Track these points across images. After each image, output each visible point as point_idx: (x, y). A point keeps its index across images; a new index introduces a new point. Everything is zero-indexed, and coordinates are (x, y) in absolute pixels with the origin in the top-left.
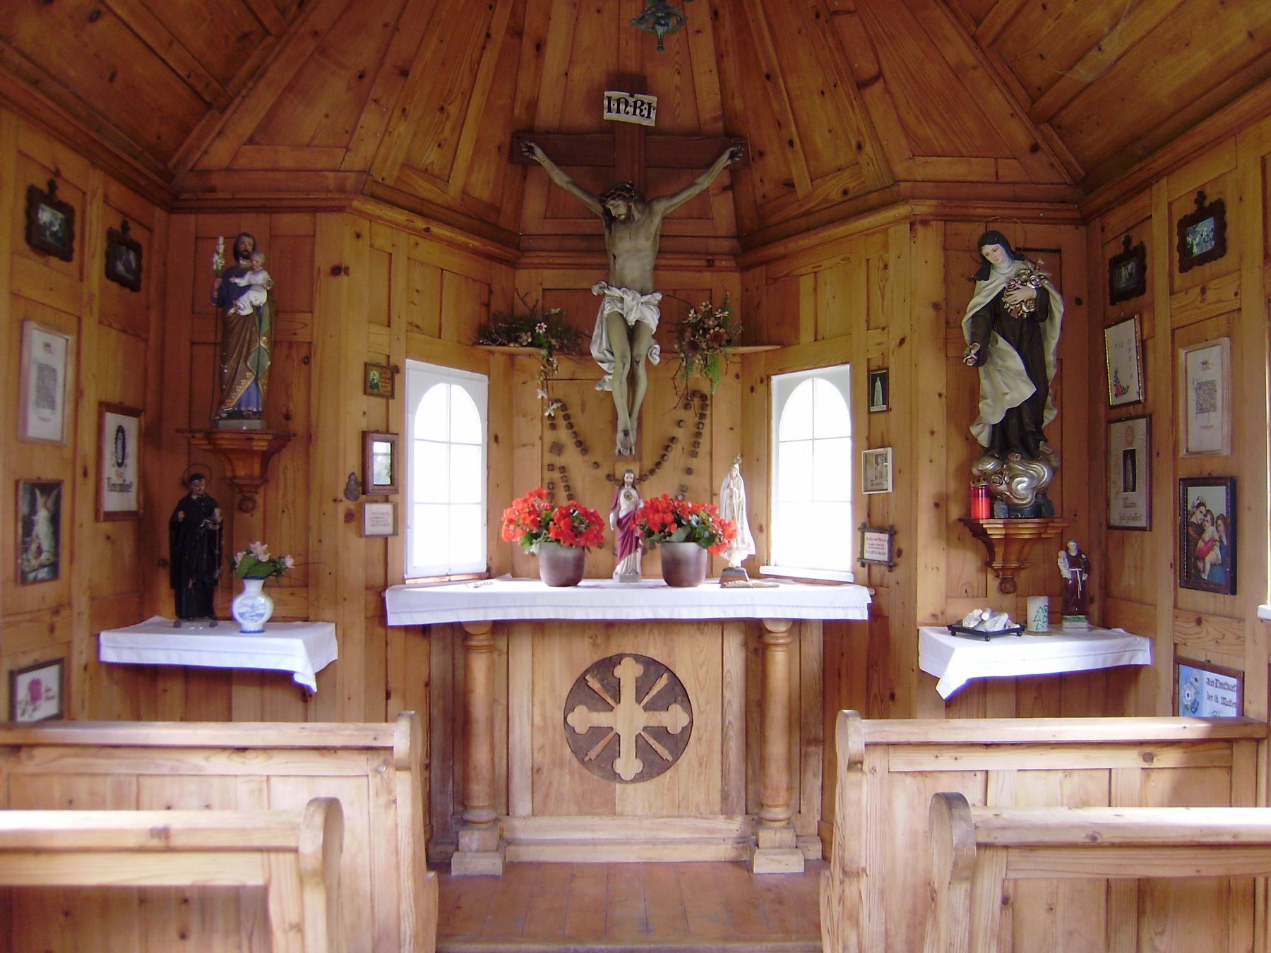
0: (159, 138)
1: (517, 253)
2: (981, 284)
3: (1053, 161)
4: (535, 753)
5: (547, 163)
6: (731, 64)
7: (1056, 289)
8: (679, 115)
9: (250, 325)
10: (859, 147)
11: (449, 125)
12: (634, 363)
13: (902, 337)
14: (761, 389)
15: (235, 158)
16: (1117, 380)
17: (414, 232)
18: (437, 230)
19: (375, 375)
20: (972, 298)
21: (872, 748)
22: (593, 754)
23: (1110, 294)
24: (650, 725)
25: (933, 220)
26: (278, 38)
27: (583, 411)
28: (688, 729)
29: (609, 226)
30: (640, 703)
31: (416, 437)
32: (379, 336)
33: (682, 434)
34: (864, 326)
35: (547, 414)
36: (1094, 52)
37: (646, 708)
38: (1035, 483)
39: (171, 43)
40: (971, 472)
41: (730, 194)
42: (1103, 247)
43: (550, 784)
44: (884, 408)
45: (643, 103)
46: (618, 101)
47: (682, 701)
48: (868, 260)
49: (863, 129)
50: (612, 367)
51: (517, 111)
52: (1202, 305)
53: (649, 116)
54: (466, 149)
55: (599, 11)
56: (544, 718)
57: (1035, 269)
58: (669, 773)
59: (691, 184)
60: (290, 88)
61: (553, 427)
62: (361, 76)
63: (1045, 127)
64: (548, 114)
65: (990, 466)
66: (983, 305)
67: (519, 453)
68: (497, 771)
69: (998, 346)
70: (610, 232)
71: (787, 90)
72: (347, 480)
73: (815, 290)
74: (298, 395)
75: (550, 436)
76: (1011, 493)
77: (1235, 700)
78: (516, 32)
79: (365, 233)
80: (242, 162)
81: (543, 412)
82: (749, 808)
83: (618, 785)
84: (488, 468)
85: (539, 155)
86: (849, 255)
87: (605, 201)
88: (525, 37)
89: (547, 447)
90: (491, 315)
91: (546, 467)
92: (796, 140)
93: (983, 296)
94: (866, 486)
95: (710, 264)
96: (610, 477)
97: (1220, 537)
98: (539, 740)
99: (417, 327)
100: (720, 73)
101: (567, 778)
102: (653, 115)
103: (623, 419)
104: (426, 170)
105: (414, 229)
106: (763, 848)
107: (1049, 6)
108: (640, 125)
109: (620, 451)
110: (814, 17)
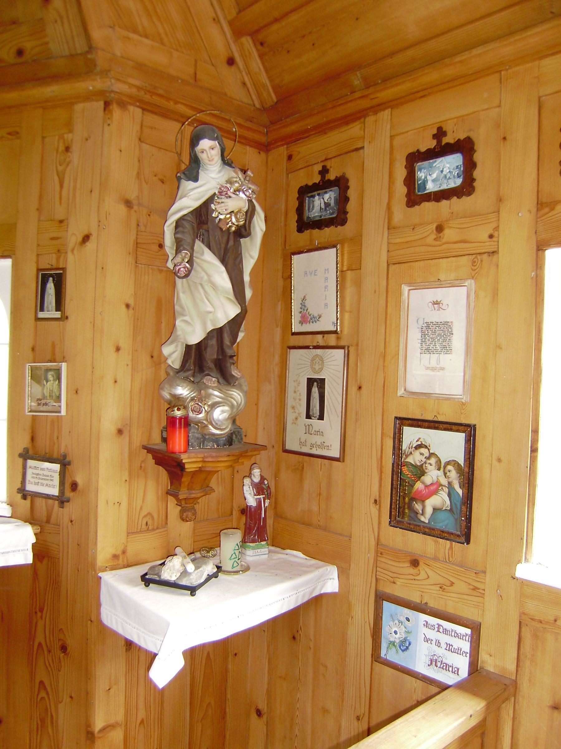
3: (247, 79)
13: (86, 232)
16: (303, 306)
25: (131, 104)
40: (161, 396)
52: (438, 243)
57: (245, 179)
63: (247, 41)
66: (191, 209)
77: (467, 649)
86: (18, 129)
97: (450, 483)
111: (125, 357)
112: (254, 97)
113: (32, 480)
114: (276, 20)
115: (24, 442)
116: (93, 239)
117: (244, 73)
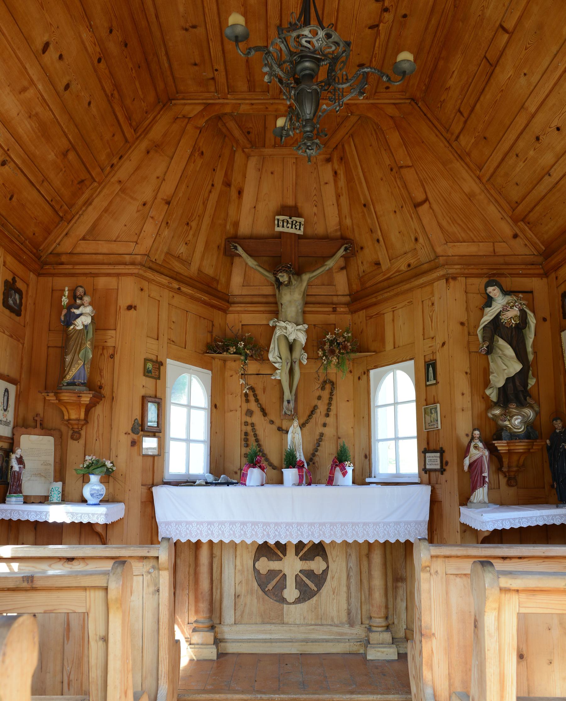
0: (34, 234)
1: (227, 304)
2: (487, 310)
3: (526, 242)
4: (237, 585)
5: (244, 255)
6: (344, 200)
7: (530, 310)
8: (316, 229)
9: (81, 335)
10: (416, 240)
11: (191, 233)
12: (292, 363)
14: (365, 377)
15: (75, 247)
17: (171, 289)
18: (185, 289)
19: (150, 365)
20: (482, 317)
21: (435, 559)
22: (270, 587)
23: (563, 313)
24: (304, 568)
25: (459, 277)
26: (100, 184)
27: (264, 392)
28: (326, 572)
29: (278, 288)
30: (297, 556)
31: (172, 436)
32: (152, 345)
33: (322, 408)
34: (422, 337)
35: (244, 392)
36: (547, 177)
37: (301, 559)
38: (526, 419)
39: (43, 181)
41: (344, 272)
42: (557, 287)
43: (245, 604)
44: (435, 382)
45: (296, 222)
46: (283, 221)
47: (322, 554)
48: (422, 301)
49: (418, 230)
50: (281, 365)
51: (228, 227)
53: (300, 229)
54: (200, 247)
55: (272, 173)
56: (242, 565)
57: (518, 300)
58: (315, 598)
59: (323, 265)
60: (106, 210)
61: (247, 401)
62: (144, 205)
63: (521, 224)
64: (245, 228)
65: (497, 412)
66: (489, 321)
67: (229, 415)
68: (214, 597)
69: (499, 343)
70: (279, 291)
71: (375, 212)
72: (133, 423)
73: (393, 320)
74: (106, 374)
75: (245, 406)
76: (512, 426)
78: (228, 184)
79: (146, 288)
80: (78, 250)
81: (242, 391)
82: (363, 620)
83: (285, 605)
84: (211, 423)
85: (240, 251)
86: (411, 300)
87: (276, 274)
88: (232, 188)
89: (244, 412)
90: (213, 338)
91: (243, 424)
92: (381, 239)
93: (489, 315)
94: (425, 426)
95: (334, 310)
96: (280, 429)
98: (239, 578)
99: (173, 341)
100: (338, 205)
101: (256, 600)
102: (302, 229)
103: (287, 395)
104: (179, 257)
105: (172, 288)
106: (372, 644)
107: (519, 155)
108: (295, 234)
109: (285, 412)
110: (389, 170)
111: (468, 397)
112: (533, 250)
113: (428, 463)
114: (530, 212)
115: (425, 446)
116: (446, 344)
117: (524, 240)
